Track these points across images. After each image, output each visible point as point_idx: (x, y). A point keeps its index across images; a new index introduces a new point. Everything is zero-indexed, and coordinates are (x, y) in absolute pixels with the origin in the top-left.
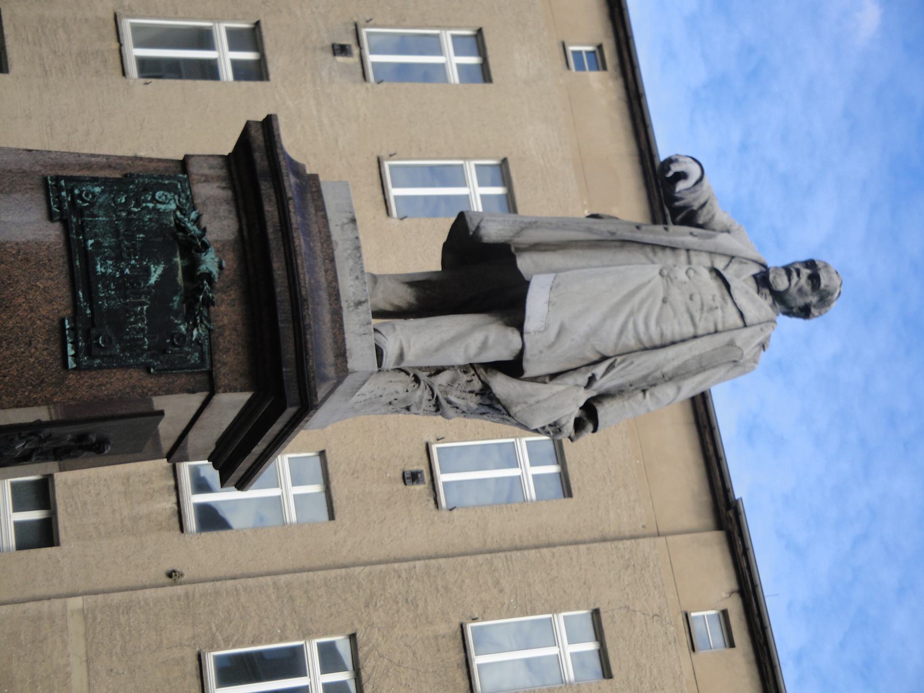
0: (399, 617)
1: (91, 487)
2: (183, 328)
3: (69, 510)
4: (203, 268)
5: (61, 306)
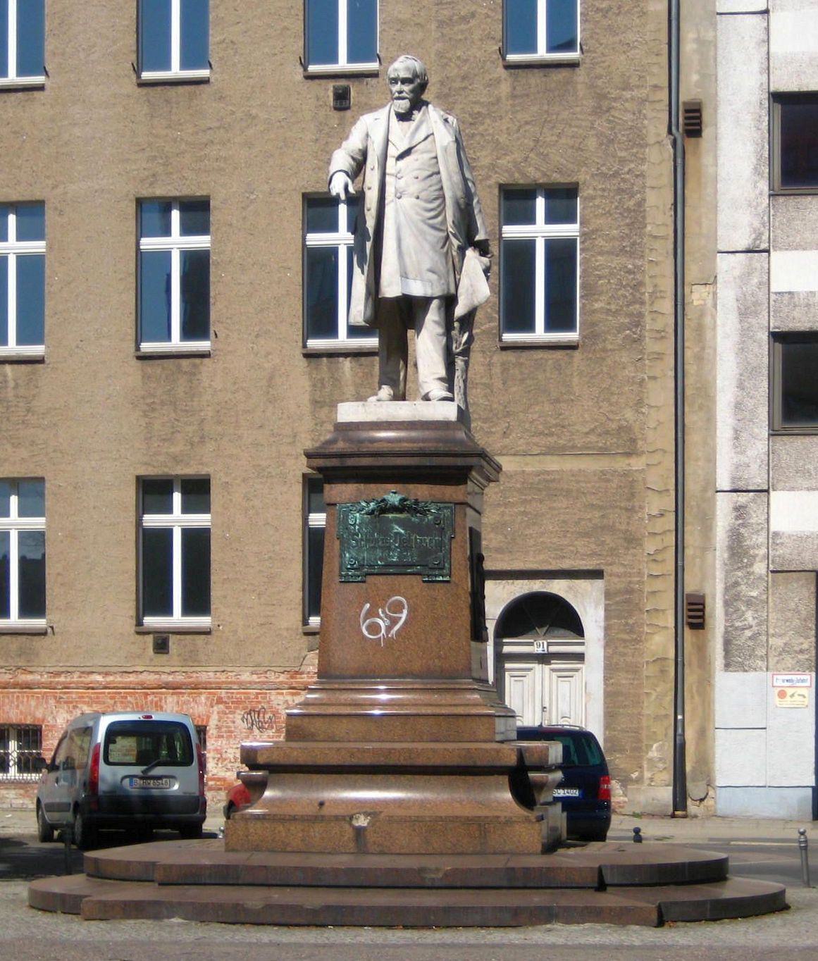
0: (489, 135)
2: (430, 517)
4: (397, 503)
5: (416, 580)
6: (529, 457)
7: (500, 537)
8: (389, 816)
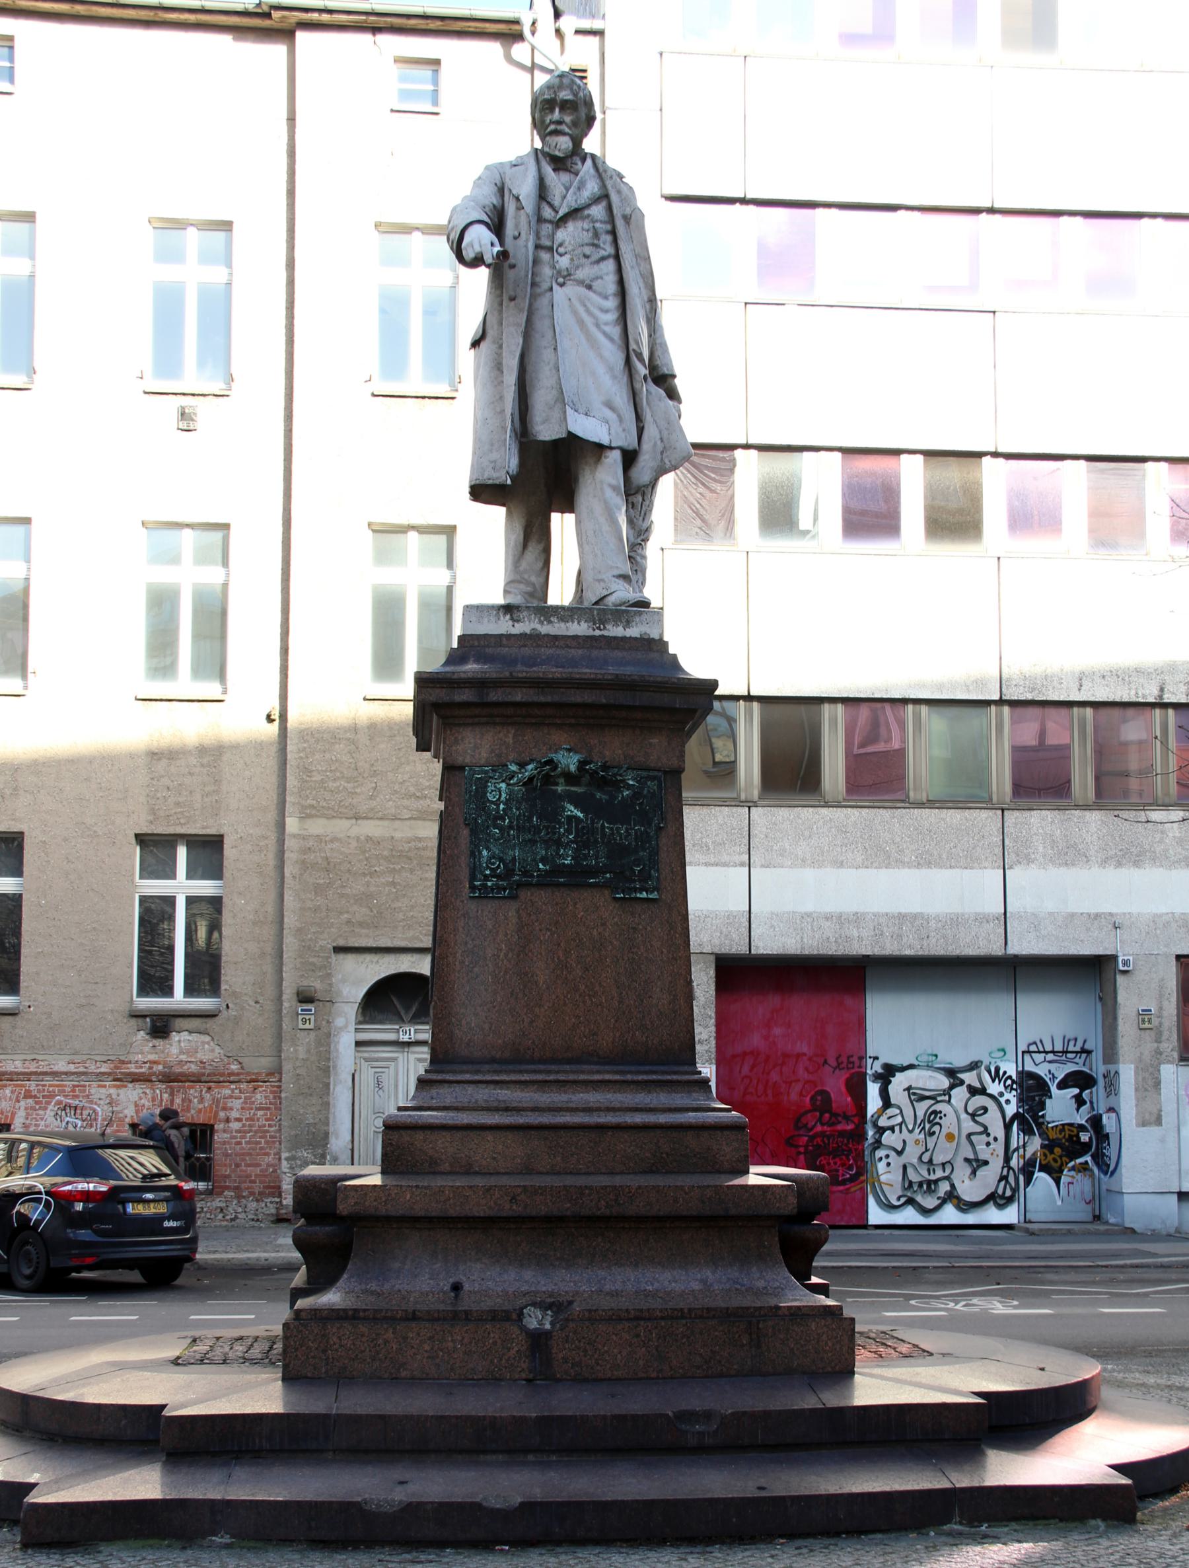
1: (159, 795)
3: (182, 821)
4: (573, 768)
5: (602, 899)
6: (398, 822)
7: (364, 910)
8: (590, 1311)
